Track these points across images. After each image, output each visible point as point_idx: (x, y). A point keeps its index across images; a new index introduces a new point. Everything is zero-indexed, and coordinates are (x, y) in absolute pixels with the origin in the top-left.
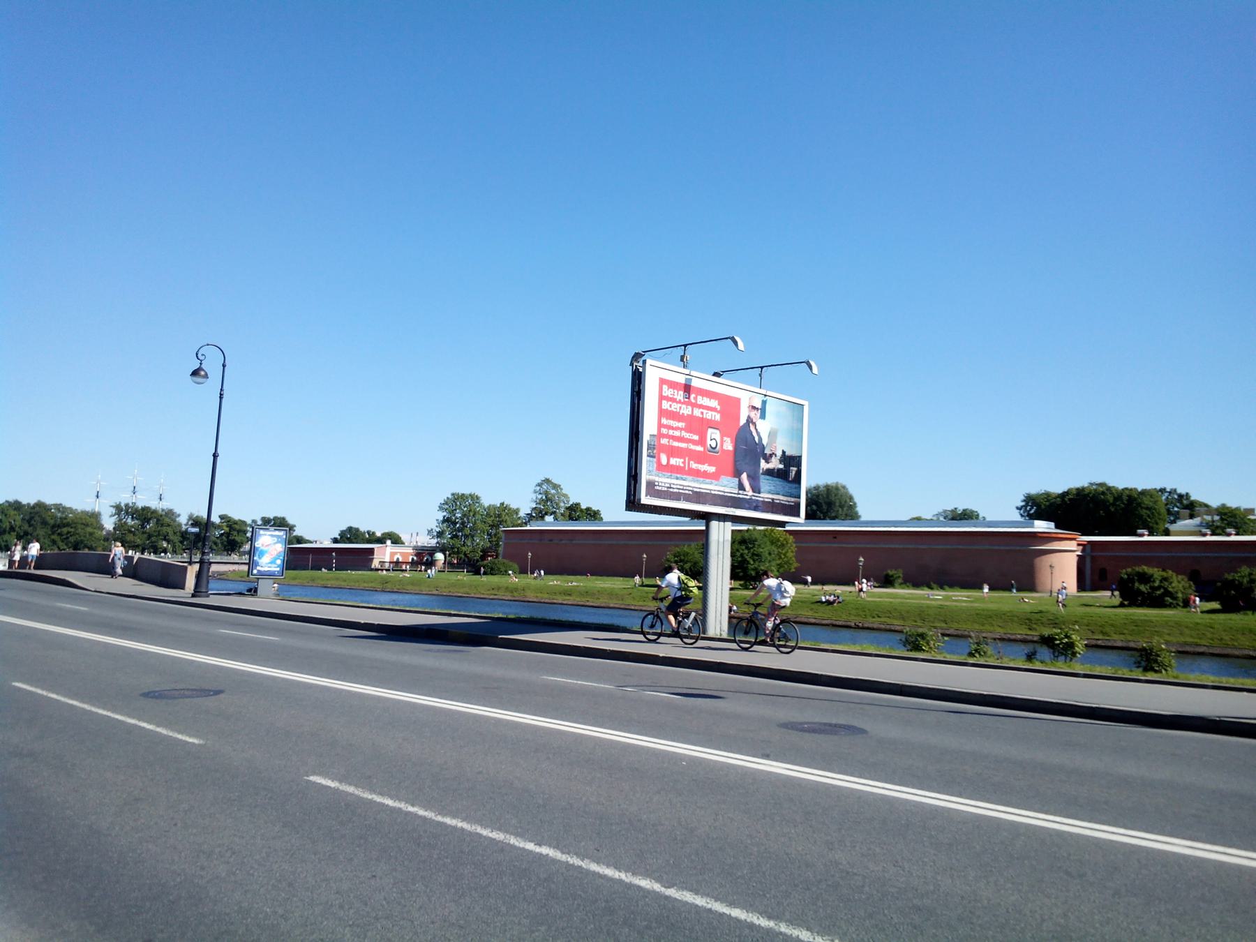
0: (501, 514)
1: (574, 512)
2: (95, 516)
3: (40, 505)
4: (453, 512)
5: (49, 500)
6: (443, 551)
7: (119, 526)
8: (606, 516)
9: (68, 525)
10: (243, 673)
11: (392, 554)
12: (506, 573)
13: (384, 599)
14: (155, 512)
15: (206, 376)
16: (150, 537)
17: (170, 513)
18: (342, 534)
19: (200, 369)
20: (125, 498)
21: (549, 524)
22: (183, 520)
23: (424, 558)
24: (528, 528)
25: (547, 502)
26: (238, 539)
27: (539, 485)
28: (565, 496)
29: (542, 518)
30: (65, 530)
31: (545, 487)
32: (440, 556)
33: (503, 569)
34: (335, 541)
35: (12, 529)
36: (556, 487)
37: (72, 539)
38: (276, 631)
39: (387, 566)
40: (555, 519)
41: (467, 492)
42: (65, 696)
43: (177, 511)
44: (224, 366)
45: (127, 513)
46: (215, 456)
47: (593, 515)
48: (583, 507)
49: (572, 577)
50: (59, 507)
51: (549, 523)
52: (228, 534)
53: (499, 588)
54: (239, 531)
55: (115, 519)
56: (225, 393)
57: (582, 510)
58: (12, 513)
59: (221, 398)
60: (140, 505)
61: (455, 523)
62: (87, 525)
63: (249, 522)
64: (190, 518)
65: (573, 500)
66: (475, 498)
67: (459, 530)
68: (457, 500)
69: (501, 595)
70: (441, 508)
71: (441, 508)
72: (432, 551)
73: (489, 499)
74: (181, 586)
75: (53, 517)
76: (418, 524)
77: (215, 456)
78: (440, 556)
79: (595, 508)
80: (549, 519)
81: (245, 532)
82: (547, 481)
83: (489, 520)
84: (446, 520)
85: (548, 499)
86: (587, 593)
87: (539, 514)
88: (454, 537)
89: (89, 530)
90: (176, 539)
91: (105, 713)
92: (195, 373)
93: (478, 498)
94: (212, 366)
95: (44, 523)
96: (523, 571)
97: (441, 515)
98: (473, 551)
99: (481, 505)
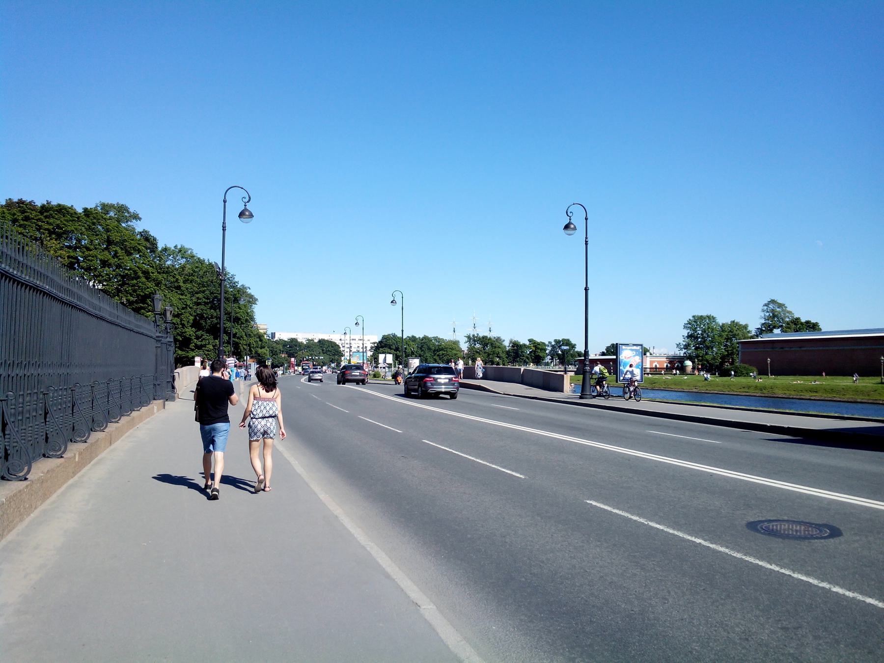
0: (733, 330)
1: (797, 325)
2: (456, 343)
3: (425, 338)
4: (695, 330)
5: (430, 335)
6: (690, 358)
7: (471, 349)
8: (824, 327)
9: (442, 349)
10: (670, 466)
11: (651, 362)
12: (748, 375)
13: (660, 395)
14: (490, 339)
15: (575, 229)
16: (489, 355)
17: (498, 339)
18: (608, 349)
19: (570, 223)
20: (472, 332)
21: (777, 335)
22: (506, 343)
23: (676, 364)
24: (760, 339)
25: (776, 316)
26: (541, 354)
27: (765, 305)
28: (790, 312)
29: (771, 331)
30: (441, 352)
31: (771, 306)
32: (688, 363)
33: (745, 372)
34: (603, 354)
35: (413, 353)
36: (781, 306)
37: (445, 358)
38: (718, 436)
39: (648, 371)
40: (782, 331)
41: (704, 314)
42: (689, 534)
43: (503, 338)
44: (586, 219)
45: (474, 341)
46: (586, 289)
47: (812, 327)
48: (803, 320)
49: (810, 378)
50: (436, 339)
51: (777, 335)
52: (535, 352)
53: (749, 387)
54: (541, 349)
55: (467, 345)
56: (589, 240)
57: (802, 324)
58: (411, 343)
59: (586, 244)
60: (481, 335)
61: (697, 338)
62: (452, 349)
63: (547, 343)
64: (511, 342)
65: (796, 316)
66: (711, 318)
67: (701, 343)
68: (695, 322)
69: (752, 392)
70: (685, 327)
71: (685, 327)
72: (681, 360)
73: (723, 318)
74: (561, 390)
75: (434, 345)
76: (669, 341)
77: (586, 289)
78: (688, 363)
79: (813, 321)
80: (777, 331)
81: (545, 350)
82: (773, 301)
83: (725, 334)
84: (689, 336)
85: (774, 316)
86: (832, 390)
87: (768, 328)
88: (696, 349)
89: (454, 352)
90: (504, 356)
91: (661, 527)
92: (567, 227)
93: (714, 318)
94: (578, 221)
95: (429, 349)
96: (762, 372)
97: (686, 332)
98: (714, 359)
99: (717, 324)
